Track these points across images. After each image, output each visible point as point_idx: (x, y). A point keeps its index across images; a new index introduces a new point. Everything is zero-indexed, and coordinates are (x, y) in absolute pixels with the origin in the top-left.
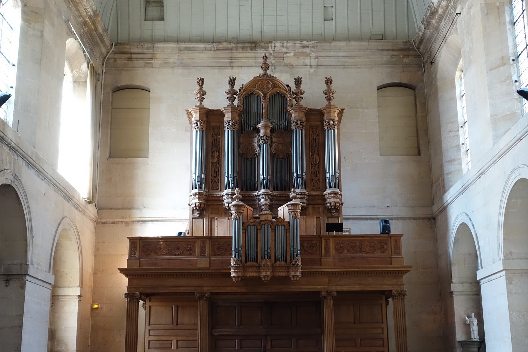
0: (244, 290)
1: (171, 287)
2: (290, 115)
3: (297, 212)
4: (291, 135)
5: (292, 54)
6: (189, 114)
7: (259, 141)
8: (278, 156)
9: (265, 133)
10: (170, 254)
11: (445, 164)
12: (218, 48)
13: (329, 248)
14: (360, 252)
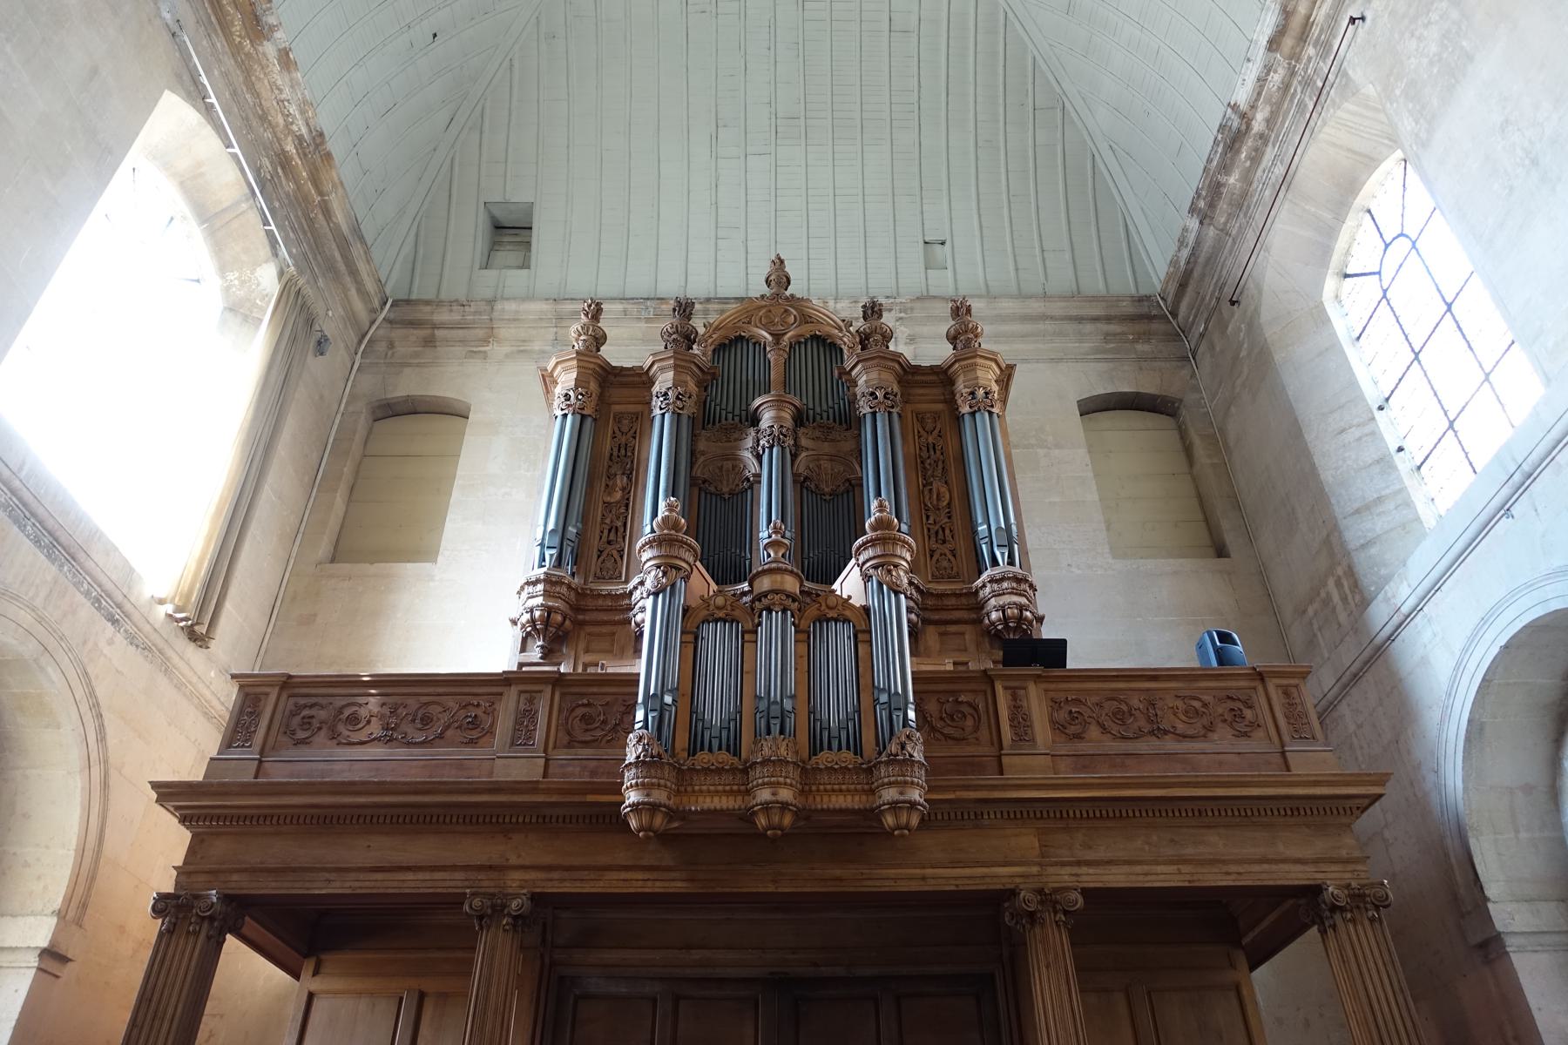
0: (679, 887)
3: (896, 566)
6: (548, 380)
8: (817, 486)
9: (778, 419)
10: (389, 741)
11: (1343, 523)
12: (659, 313)
13: (1027, 718)
14: (1152, 733)
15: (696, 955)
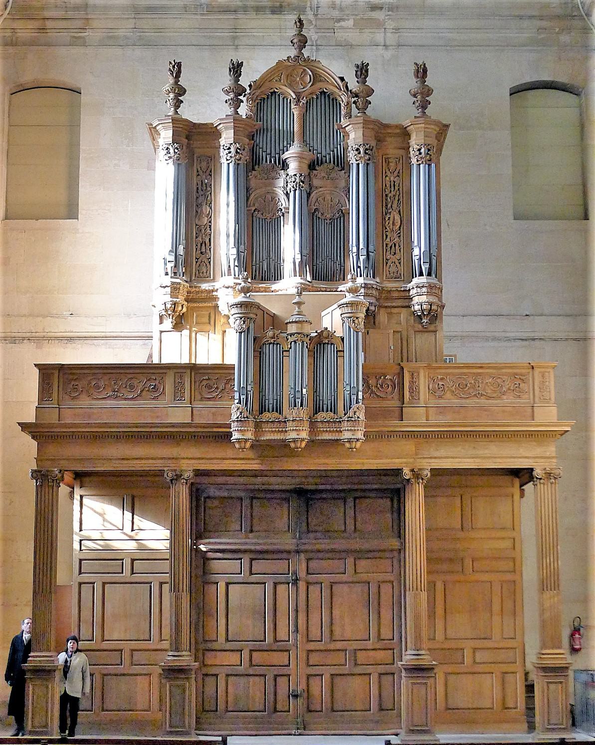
1: (119, 459)
2: (347, 135)
4: (347, 175)
5: (350, 23)
7: (287, 186)
15: (259, 479)
